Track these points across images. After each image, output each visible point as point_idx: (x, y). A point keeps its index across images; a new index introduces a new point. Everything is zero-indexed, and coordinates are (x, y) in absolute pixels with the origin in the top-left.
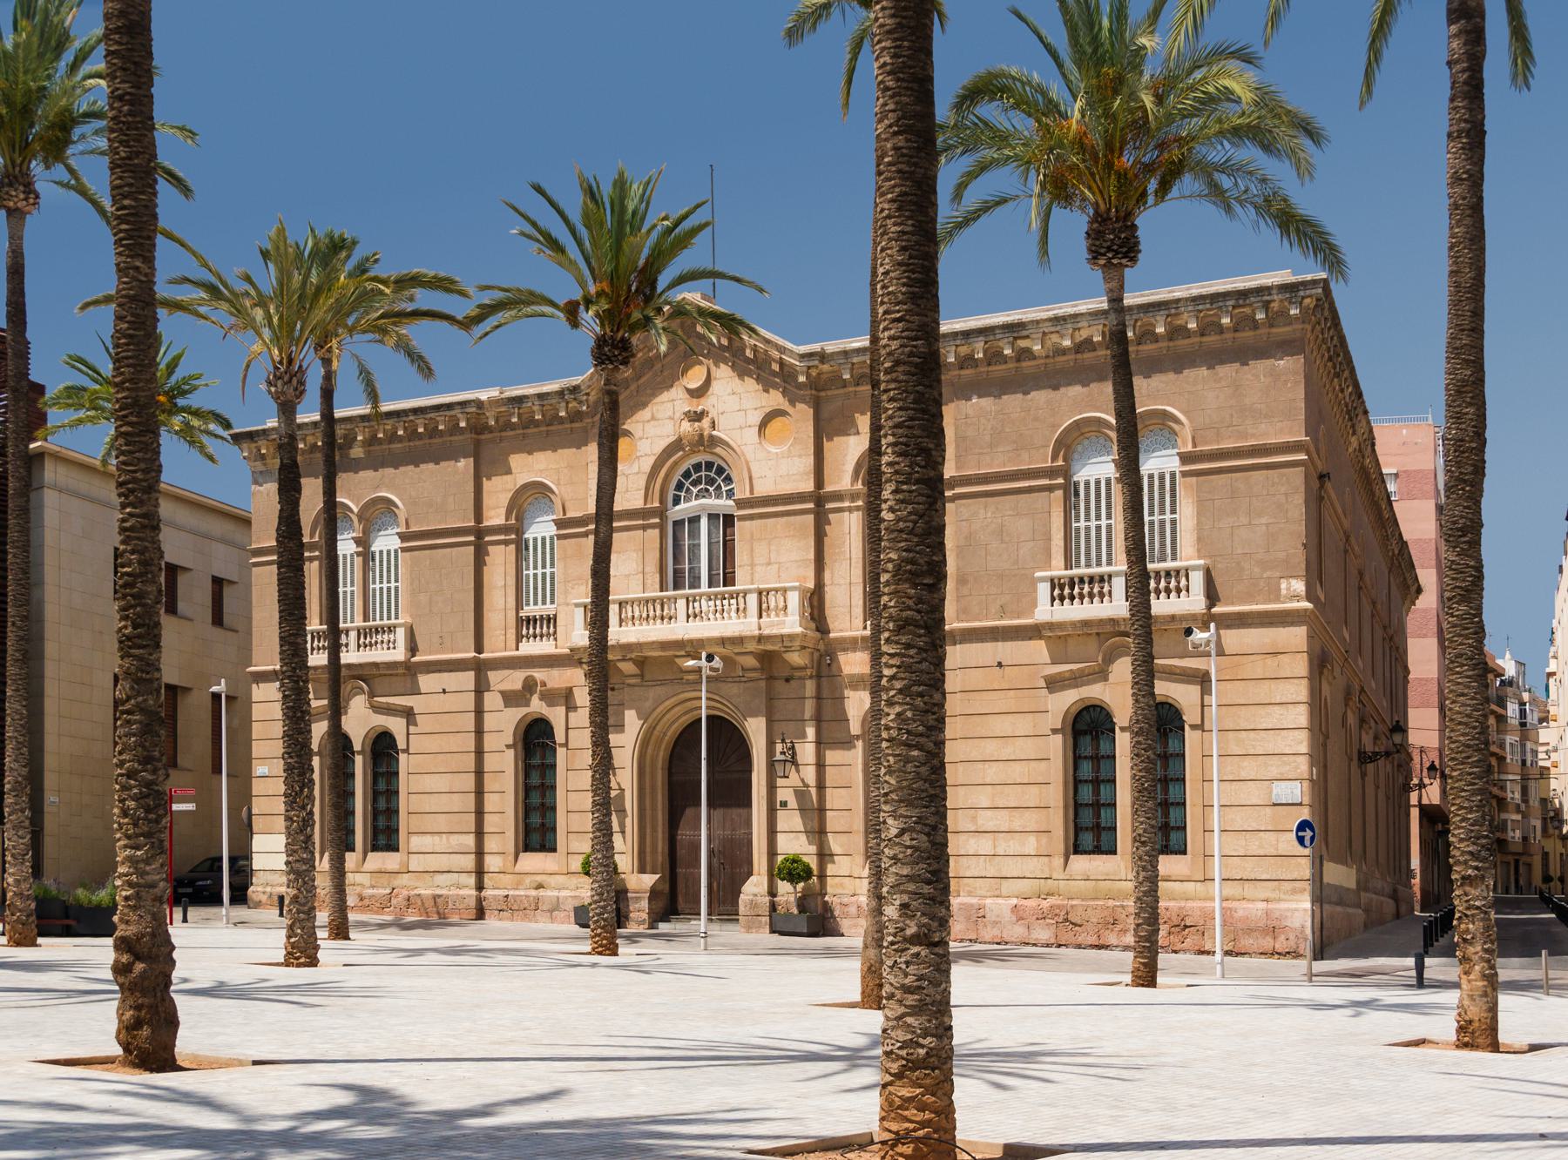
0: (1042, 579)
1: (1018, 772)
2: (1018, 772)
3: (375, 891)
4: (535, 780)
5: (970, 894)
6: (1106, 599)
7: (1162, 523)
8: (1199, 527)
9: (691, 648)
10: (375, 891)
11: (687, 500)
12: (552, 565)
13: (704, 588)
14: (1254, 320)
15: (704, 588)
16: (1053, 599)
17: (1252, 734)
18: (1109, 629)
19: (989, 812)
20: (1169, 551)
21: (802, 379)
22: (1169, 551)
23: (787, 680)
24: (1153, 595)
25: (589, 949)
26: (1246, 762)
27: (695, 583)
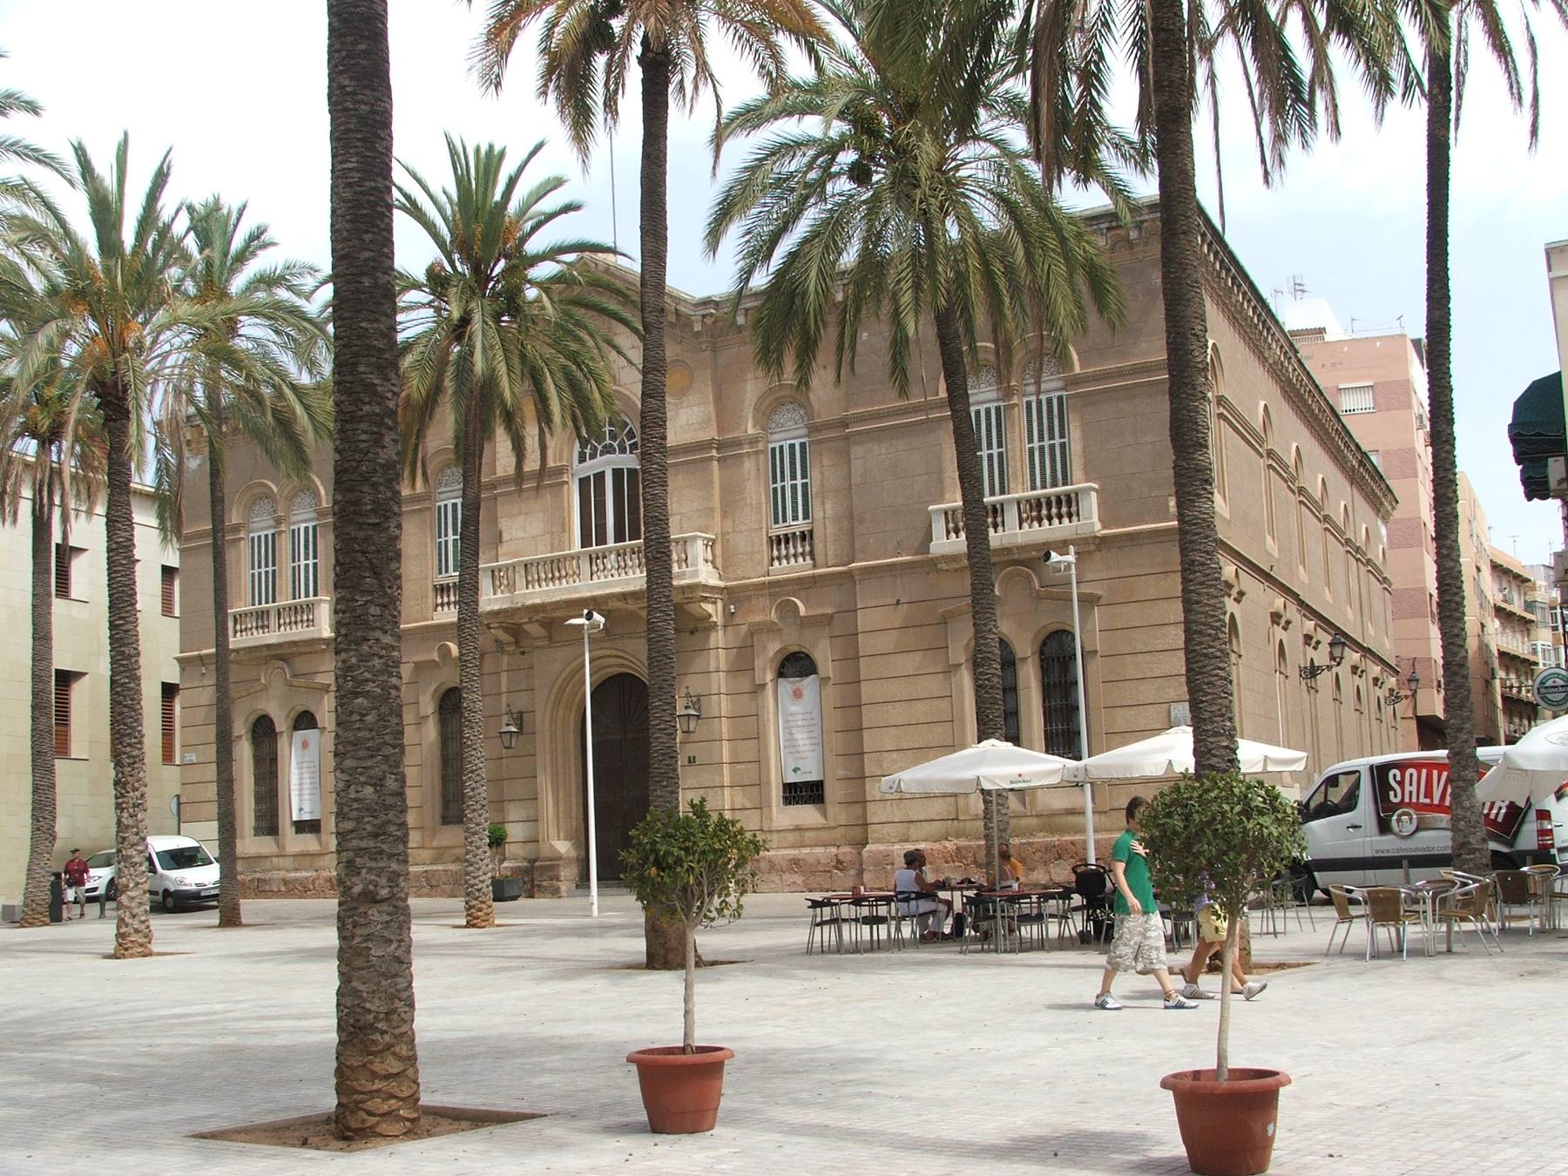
0: (937, 511)
1: (920, 711)
2: (920, 711)
3: (298, 874)
4: (1055, 676)
5: (878, 841)
6: (1075, 518)
7: (1052, 447)
8: (1086, 451)
9: (575, 606)
10: (298, 874)
11: (593, 456)
12: (1031, 451)
13: (611, 544)
14: (1129, 241)
15: (611, 544)
16: (948, 533)
17: (1148, 657)
18: (265, 653)
19: (894, 755)
20: (1059, 476)
21: (697, 327)
22: (1059, 476)
23: (692, 633)
24: (991, 530)
25: (464, 922)
26: (1143, 687)
27: (602, 540)
